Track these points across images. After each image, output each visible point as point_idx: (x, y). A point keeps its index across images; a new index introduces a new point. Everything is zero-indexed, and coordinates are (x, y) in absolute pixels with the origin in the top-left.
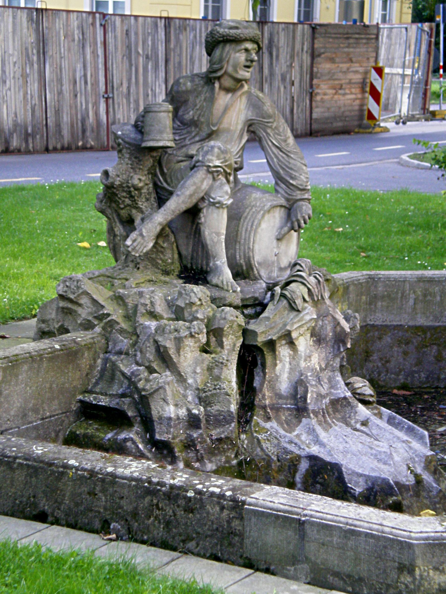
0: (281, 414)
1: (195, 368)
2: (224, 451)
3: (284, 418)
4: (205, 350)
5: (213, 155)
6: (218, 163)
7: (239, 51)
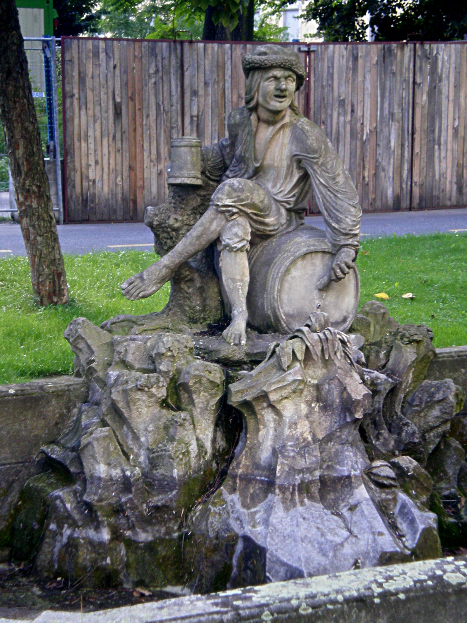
0: (251, 486)
1: (148, 426)
2: (166, 522)
3: (252, 491)
4: (164, 404)
5: (222, 194)
7: (268, 79)
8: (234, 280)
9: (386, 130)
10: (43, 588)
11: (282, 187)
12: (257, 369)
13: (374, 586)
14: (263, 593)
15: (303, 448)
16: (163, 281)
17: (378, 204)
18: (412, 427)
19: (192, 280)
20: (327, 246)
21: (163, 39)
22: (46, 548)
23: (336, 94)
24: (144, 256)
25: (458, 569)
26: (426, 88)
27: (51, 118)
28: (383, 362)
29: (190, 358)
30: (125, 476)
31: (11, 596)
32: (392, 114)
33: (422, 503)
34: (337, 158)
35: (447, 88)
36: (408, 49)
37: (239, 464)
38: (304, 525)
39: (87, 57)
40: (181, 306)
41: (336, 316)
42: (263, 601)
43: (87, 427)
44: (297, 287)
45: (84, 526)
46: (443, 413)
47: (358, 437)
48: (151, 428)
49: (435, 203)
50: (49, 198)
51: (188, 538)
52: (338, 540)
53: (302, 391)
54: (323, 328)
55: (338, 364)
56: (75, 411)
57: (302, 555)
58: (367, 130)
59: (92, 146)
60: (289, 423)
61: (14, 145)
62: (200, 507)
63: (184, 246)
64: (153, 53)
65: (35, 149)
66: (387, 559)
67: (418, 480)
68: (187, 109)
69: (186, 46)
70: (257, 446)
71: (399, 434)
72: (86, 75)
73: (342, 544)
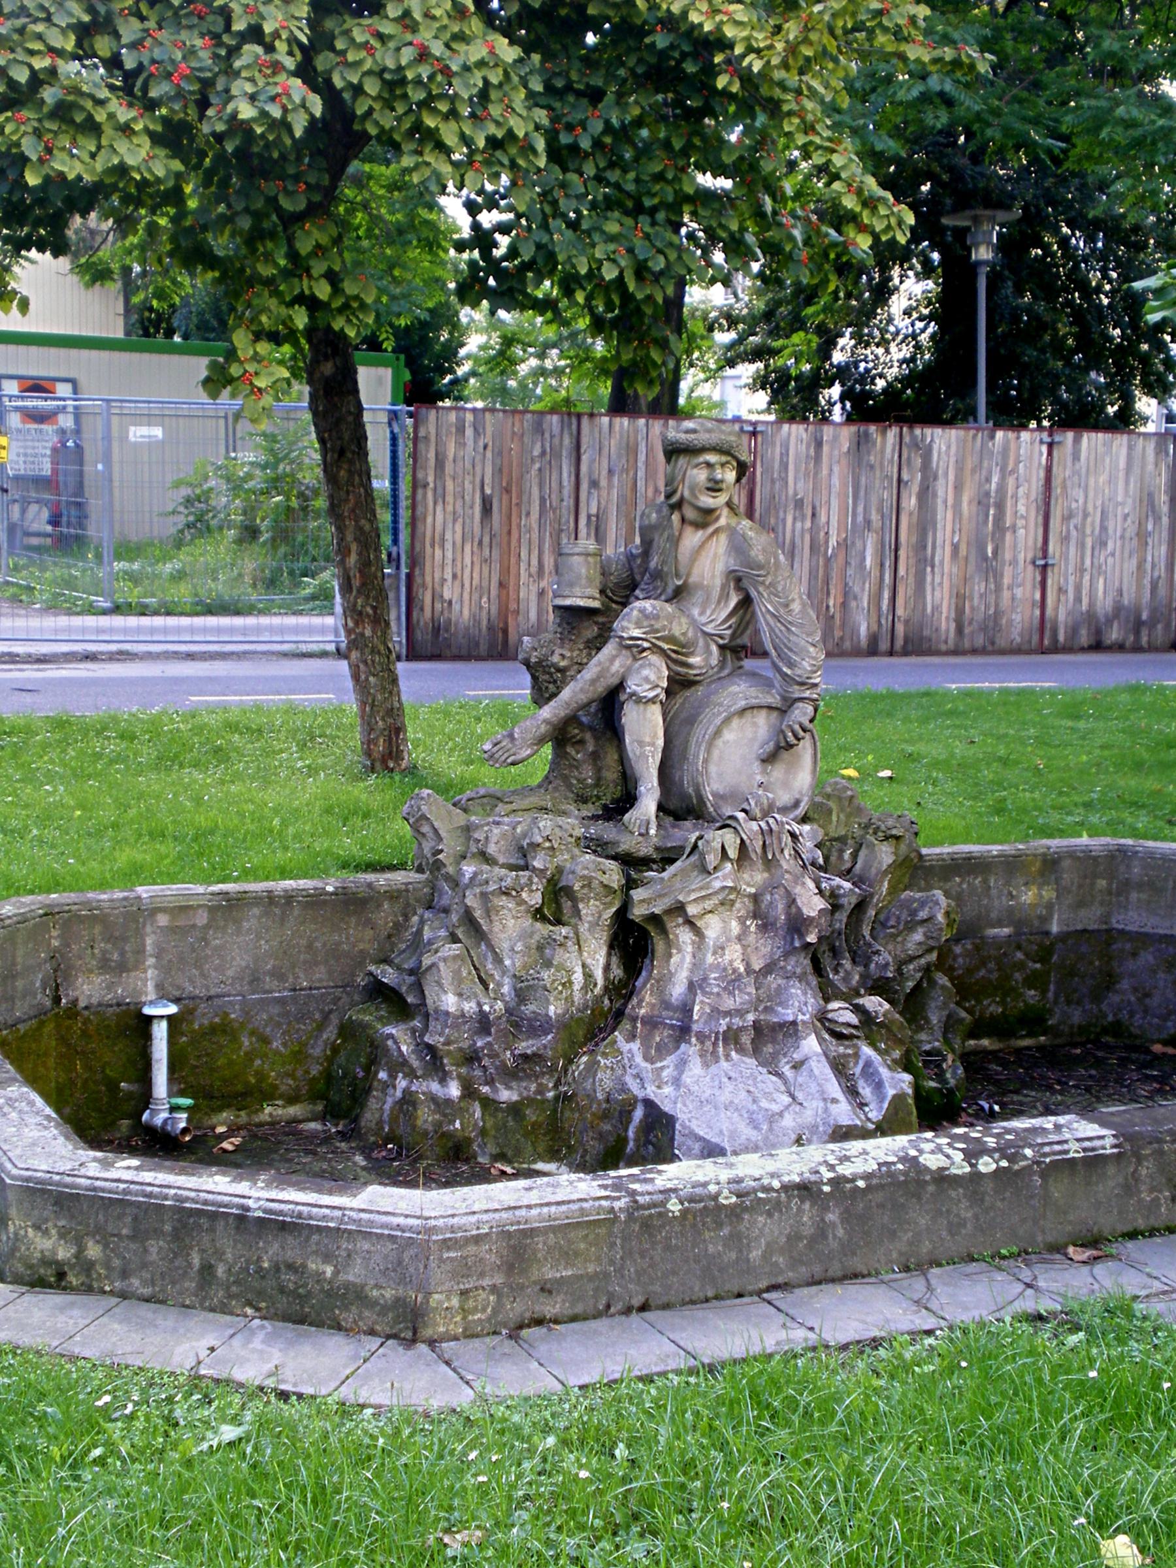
4: (538, 914)
6: (636, 633)
8: (641, 744)
9: (859, 544)
10: (368, 1158)
11: (714, 615)
12: (672, 869)
13: (823, 1169)
14: (670, 1175)
15: (732, 982)
16: (541, 741)
17: (847, 645)
18: (884, 957)
19: (581, 742)
20: (774, 699)
21: (553, 411)
22: (373, 1104)
23: (791, 492)
24: (515, 708)
25: (939, 1149)
26: (915, 488)
27: (395, 516)
28: (848, 865)
29: (576, 851)
30: (481, 1011)
31: (325, 1166)
32: (868, 522)
33: (894, 1061)
34: (790, 577)
35: (944, 489)
36: (892, 433)
37: (641, 1001)
38: (729, 1086)
39: (449, 433)
40: (566, 778)
41: (784, 798)
42: (669, 1185)
43: (430, 942)
44: (730, 756)
45: (425, 1077)
46: (927, 937)
47: (809, 969)
48: (519, 947)
49: (925, 646)
50: (387, 624)
51: (567, 1098)
52: (776, 1108)
53: (733, 902)
54: (766, 814)
55: (785, 866)
56: (415, 919)
57: (725, 1126)
58: (833, 542)
59: (449, 554)
60: (714, 946)
61: (343, 551)
62: (585, 1059)
63: (571, 694)
64: (539, 429)
66: (842, 1134)
67: (889, 1030)
68: (583, 505)
69: (585, 421)
70: (665, 980)
71: (866, 966)
72: (445, 456)
73: (781, 1114)
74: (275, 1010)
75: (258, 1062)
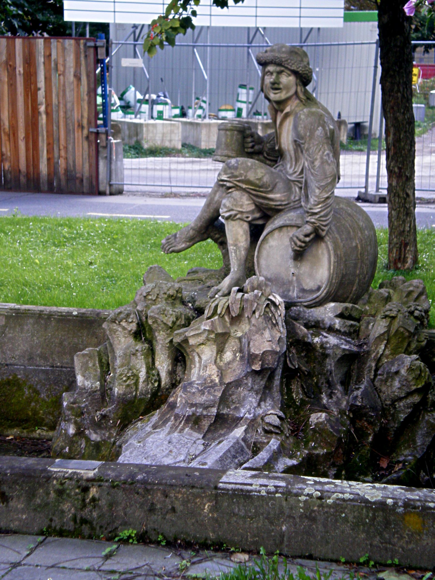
65: (402, 136)
74: (42, 376)
75: (33, 404)
